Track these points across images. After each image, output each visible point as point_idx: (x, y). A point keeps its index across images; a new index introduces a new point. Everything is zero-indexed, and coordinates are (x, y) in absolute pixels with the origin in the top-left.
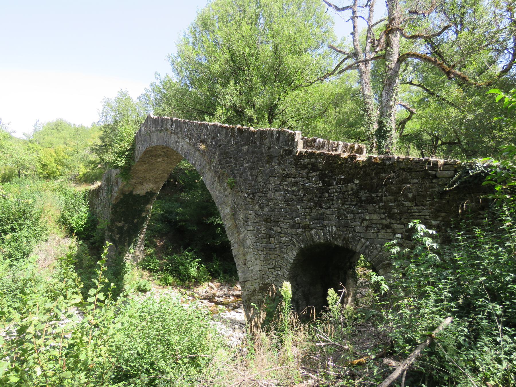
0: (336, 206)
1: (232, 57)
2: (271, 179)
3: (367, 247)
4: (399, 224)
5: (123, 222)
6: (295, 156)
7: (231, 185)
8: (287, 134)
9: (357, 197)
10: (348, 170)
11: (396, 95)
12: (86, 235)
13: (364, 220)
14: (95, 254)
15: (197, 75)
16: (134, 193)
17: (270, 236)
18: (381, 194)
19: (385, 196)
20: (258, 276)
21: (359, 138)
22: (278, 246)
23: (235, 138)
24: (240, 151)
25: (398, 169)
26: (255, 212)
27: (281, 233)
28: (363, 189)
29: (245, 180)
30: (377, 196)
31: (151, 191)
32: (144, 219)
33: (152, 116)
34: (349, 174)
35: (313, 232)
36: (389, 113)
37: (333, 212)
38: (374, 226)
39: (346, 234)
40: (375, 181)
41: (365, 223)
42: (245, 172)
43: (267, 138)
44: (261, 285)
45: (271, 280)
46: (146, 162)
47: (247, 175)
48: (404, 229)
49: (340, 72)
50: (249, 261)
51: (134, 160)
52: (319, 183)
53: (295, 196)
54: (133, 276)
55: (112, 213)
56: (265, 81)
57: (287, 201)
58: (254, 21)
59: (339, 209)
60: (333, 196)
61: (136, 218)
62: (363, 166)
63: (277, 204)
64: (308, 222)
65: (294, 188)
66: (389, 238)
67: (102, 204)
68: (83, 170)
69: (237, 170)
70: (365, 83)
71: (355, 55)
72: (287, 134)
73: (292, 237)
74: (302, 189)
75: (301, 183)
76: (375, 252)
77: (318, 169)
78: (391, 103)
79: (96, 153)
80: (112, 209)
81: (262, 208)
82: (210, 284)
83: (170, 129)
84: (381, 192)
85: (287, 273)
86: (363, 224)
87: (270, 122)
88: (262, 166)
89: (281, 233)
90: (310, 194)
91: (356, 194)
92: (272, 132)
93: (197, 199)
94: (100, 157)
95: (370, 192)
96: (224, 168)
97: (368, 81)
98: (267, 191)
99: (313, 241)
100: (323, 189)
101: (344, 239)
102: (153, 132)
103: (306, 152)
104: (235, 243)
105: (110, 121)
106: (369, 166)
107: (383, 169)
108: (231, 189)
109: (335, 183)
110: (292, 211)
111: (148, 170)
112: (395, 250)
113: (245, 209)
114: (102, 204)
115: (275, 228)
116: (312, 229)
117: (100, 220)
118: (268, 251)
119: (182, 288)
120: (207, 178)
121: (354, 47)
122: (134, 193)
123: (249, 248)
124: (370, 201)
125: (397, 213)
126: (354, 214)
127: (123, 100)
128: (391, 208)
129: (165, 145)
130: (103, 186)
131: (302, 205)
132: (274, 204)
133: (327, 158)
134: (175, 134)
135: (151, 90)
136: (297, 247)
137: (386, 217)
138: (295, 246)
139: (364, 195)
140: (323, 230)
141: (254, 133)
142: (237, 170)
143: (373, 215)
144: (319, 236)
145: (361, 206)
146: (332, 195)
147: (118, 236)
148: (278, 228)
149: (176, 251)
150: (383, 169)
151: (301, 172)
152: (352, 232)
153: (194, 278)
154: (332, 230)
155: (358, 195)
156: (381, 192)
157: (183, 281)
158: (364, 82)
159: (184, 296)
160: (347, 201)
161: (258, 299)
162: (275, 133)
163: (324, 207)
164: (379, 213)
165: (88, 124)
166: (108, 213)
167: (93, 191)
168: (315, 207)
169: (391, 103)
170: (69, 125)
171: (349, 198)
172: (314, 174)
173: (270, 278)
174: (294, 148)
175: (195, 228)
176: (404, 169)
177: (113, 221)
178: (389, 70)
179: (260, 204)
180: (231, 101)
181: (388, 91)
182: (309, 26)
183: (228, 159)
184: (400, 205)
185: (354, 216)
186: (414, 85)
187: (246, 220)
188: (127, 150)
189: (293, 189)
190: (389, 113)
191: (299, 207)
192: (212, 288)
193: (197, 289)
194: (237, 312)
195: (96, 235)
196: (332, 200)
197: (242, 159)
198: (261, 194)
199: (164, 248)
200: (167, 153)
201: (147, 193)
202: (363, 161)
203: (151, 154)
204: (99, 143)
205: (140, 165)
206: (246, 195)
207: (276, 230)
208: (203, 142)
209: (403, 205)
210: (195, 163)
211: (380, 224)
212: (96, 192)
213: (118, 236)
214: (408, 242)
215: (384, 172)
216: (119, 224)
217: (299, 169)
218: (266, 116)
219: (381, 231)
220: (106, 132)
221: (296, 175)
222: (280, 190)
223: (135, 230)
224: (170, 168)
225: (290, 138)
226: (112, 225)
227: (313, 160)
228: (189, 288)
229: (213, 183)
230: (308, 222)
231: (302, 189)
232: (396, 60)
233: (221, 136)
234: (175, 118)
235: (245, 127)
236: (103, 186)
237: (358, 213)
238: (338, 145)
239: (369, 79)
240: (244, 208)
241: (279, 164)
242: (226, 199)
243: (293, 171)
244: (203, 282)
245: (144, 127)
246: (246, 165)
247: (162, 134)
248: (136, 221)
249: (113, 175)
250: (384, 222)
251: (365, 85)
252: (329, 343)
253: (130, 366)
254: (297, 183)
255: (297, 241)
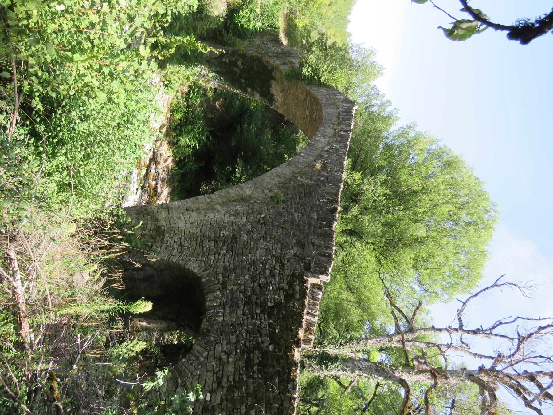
0: (246, 321)
1: (415, 192)
2: (280, 245)
3: (198, 358)
4: (221, 397)
5: (242, 67)
6: (303, 274)
7: (275, 197)
8: (327, 266)
9: (254, 348)
10: (285, 337)
11: (365, 377)
12: (229, 25)
13: (228, 355)
14: (208, 34)
15: (395, 154)
16: (272, 81)
17: (216, 242)
18: (256, 377)
19: (253, 383)
20: (173, 225)
21: (323, 322)
22: (206, 250)
23: (326, 203)
24: (311, 209)
25: (283, 398)
26: (244, 225)
27: (219, 254)
28: (263, 355)
29: (280, 214)
30: (254, 372)
31: (274, 100)
32: (245, 90)
33: (354, 108)
34: (280, 339)
35: (218, 293)
36: (346, 368)
37: (239, 318)
38: (221, 367)
39: (213, 333)
40: (271, 370)
41: (224, 357)
42: (288, 214)
43: (324, 241)
44: (163, 228)
45: (167, 241)
46: (305, 98)
47: (284, 217)
48: (215, 404)
49: (393, 312)
50: (190, 215)
51: (308, 84)
52: (271, 303)
53: (259, 273)
54: (183, 76)
55: (252, 56)
56: (388, 225)
57: (254, 264)
58: (452, 217)
59: (242, 325)
60: (256, 319)
61: (245, 82)
62: (288, 356)
63: (252, 252)
64: (229, 288)
65: (267, 272)
66: (206, 385)
67: (263, 46)
68: (301, 23)
69: (291, 205)
70: (380, 340)
71: (411, 330)
72: (327, 266)
73: (214, 268)
74: (267, 282)
75: (273, 281)
76: (191, 368)
77: (287, 301)
78: (357, 372)
79: (318, 39)
80: (256, 56)
81: (248, 233)
82: (170, 159)
83: (339, 128)
84: (258, 377)
85: (174, 261)
86: (223, 354)
87: (344, 232)
88: (294, 235)
89: (219, 254)
90: (260, 291)
91: (258, 346)
92: (330, 248)
93: (264, 148)
94: (313, 43)
95: (259, 364)
96: (294, 189)
97: (381, 344)
98: (266, 240)
99: (208, 292)
100: (265, 306)
101: (209, 331)
102: (338, 108)
103: (307, 288)
104: (211, 198)
105: (353, 55)
106: (288, 363)
107: (284, 380)
108: (271, 197)
109: (271, 321)
110: (242, 269)
111: (297, 98)
112: (191, 397)
113: (248, 213)
114: (263, 46)
115: (225, 247)
116: (221, 291)
117: (246, 43)
118: (199, 239)
119: (167, 128)
120: (284, 170)
121: (419, 329)
122: (272, 81)
123: (205, 216)
124: (249, 363)
125: (234, 396)
126: (236, 343)
127: (373, 71)
128: (239, 388)
129: (323, 121)
130: (282, 47)
131: (249, 282)
132: (251, 248)
133: (299, 313)
134: (335, 134)
135: (383, 100)
136: (203, 273)
137: (230, 382)
138: (204, 271)
139: (256, 356)
140: (220, 305)
141: (330, 226)
142: (291, 205)
143: (233, 366)
144: (213, 300)
145: (244, 353)
146: (258, 318)
147: (227, 61)
148: (225, 252)
149: (209, 122)
150: (284, 380)
151: (285, 281)
152: (215, 341)
153: (178, 141)
154: (220, 316)
155: (256, 349)
156: (258, 377)
157: (175, 129)
158: (381, 339)
159: (158, 131)
160: (250, 336)
161: (147, 224)
162: (329, 251)
163: (245, 308)
164: (235, 374)
165: (350, 28)
166: (252, 52)
167: (278, 36)
168: (246, 297)
169: (357, 372)
170: (350, 9)
171: (254, 337)
172: (282, 297)
173: (170, 240)
174: (312, 273)
175: (233, 144)
176: (282, 405)
177: (243, 56)
178: (393, 370)
179: (252, 231)
180: (367, 190)
181: (370, 368)
182: (443, 277)
183: (303, 195)
184: (242, 400)
185: (233, 344)
186: (376, 389)
187: (236, 214)
188: (319, 78)
189: (267, 271)
190: (346, 368)
191: (247, 277)
192: (166, 160)
193: (166, 145)
194: (137, 189)
195: (228, 37)
196: (252, 318)
197: (303, 211)
198: (263, 233)
199: (212, 108)
200: (314, 124)
201: (273, 95)
202: (293, 356)
203: (314, 104)
204: (329, 43)
205: (303, 91)
206: (263, 216)
207: (223, 249)
208: (324, 167)
209: (243, 403)
210: (302, 156)
211: (222, 374)
212: (276, 40)
213: (227, 61)
214: (201, 408)
215: (280, 382)
216: (240, 63)
217: (288, 279)
218: (349, 228)
219: (215, 375)
220: (341, 49)
221: (282, 274)
222: (266, 255)
223: (233, 79)
224: (298, 123)
225: (323, 269)
226: (239, 55)
227: (298, 296)
228: (167, 136)
229: (278, 176)
230: (229, 288)
231: (267, 282)
232: (403, 378)
233: (329, 188)
234: (351, 134)
235: (337, 215)
236: (282, 47)
237: (236, 349)
238: (314, 316)
239: (384, 344)
240: (250, 211)
241: (295, 255)
242: (260, 190)
243: (287, 272)
244: (173, 151)
245: (343, 98)
246: (296, 216)
247: (335, 119)
248: (243, 81)
249: (293, 60)
250: (225, 380)
251: (378, 340)
252: (80, 348)
253: (62, 117)
254: (273, 275)
255: (209, 273)
